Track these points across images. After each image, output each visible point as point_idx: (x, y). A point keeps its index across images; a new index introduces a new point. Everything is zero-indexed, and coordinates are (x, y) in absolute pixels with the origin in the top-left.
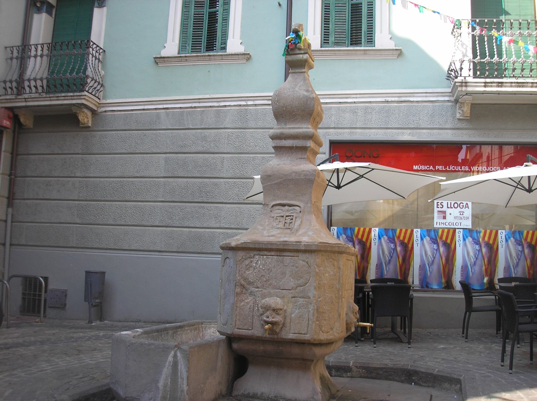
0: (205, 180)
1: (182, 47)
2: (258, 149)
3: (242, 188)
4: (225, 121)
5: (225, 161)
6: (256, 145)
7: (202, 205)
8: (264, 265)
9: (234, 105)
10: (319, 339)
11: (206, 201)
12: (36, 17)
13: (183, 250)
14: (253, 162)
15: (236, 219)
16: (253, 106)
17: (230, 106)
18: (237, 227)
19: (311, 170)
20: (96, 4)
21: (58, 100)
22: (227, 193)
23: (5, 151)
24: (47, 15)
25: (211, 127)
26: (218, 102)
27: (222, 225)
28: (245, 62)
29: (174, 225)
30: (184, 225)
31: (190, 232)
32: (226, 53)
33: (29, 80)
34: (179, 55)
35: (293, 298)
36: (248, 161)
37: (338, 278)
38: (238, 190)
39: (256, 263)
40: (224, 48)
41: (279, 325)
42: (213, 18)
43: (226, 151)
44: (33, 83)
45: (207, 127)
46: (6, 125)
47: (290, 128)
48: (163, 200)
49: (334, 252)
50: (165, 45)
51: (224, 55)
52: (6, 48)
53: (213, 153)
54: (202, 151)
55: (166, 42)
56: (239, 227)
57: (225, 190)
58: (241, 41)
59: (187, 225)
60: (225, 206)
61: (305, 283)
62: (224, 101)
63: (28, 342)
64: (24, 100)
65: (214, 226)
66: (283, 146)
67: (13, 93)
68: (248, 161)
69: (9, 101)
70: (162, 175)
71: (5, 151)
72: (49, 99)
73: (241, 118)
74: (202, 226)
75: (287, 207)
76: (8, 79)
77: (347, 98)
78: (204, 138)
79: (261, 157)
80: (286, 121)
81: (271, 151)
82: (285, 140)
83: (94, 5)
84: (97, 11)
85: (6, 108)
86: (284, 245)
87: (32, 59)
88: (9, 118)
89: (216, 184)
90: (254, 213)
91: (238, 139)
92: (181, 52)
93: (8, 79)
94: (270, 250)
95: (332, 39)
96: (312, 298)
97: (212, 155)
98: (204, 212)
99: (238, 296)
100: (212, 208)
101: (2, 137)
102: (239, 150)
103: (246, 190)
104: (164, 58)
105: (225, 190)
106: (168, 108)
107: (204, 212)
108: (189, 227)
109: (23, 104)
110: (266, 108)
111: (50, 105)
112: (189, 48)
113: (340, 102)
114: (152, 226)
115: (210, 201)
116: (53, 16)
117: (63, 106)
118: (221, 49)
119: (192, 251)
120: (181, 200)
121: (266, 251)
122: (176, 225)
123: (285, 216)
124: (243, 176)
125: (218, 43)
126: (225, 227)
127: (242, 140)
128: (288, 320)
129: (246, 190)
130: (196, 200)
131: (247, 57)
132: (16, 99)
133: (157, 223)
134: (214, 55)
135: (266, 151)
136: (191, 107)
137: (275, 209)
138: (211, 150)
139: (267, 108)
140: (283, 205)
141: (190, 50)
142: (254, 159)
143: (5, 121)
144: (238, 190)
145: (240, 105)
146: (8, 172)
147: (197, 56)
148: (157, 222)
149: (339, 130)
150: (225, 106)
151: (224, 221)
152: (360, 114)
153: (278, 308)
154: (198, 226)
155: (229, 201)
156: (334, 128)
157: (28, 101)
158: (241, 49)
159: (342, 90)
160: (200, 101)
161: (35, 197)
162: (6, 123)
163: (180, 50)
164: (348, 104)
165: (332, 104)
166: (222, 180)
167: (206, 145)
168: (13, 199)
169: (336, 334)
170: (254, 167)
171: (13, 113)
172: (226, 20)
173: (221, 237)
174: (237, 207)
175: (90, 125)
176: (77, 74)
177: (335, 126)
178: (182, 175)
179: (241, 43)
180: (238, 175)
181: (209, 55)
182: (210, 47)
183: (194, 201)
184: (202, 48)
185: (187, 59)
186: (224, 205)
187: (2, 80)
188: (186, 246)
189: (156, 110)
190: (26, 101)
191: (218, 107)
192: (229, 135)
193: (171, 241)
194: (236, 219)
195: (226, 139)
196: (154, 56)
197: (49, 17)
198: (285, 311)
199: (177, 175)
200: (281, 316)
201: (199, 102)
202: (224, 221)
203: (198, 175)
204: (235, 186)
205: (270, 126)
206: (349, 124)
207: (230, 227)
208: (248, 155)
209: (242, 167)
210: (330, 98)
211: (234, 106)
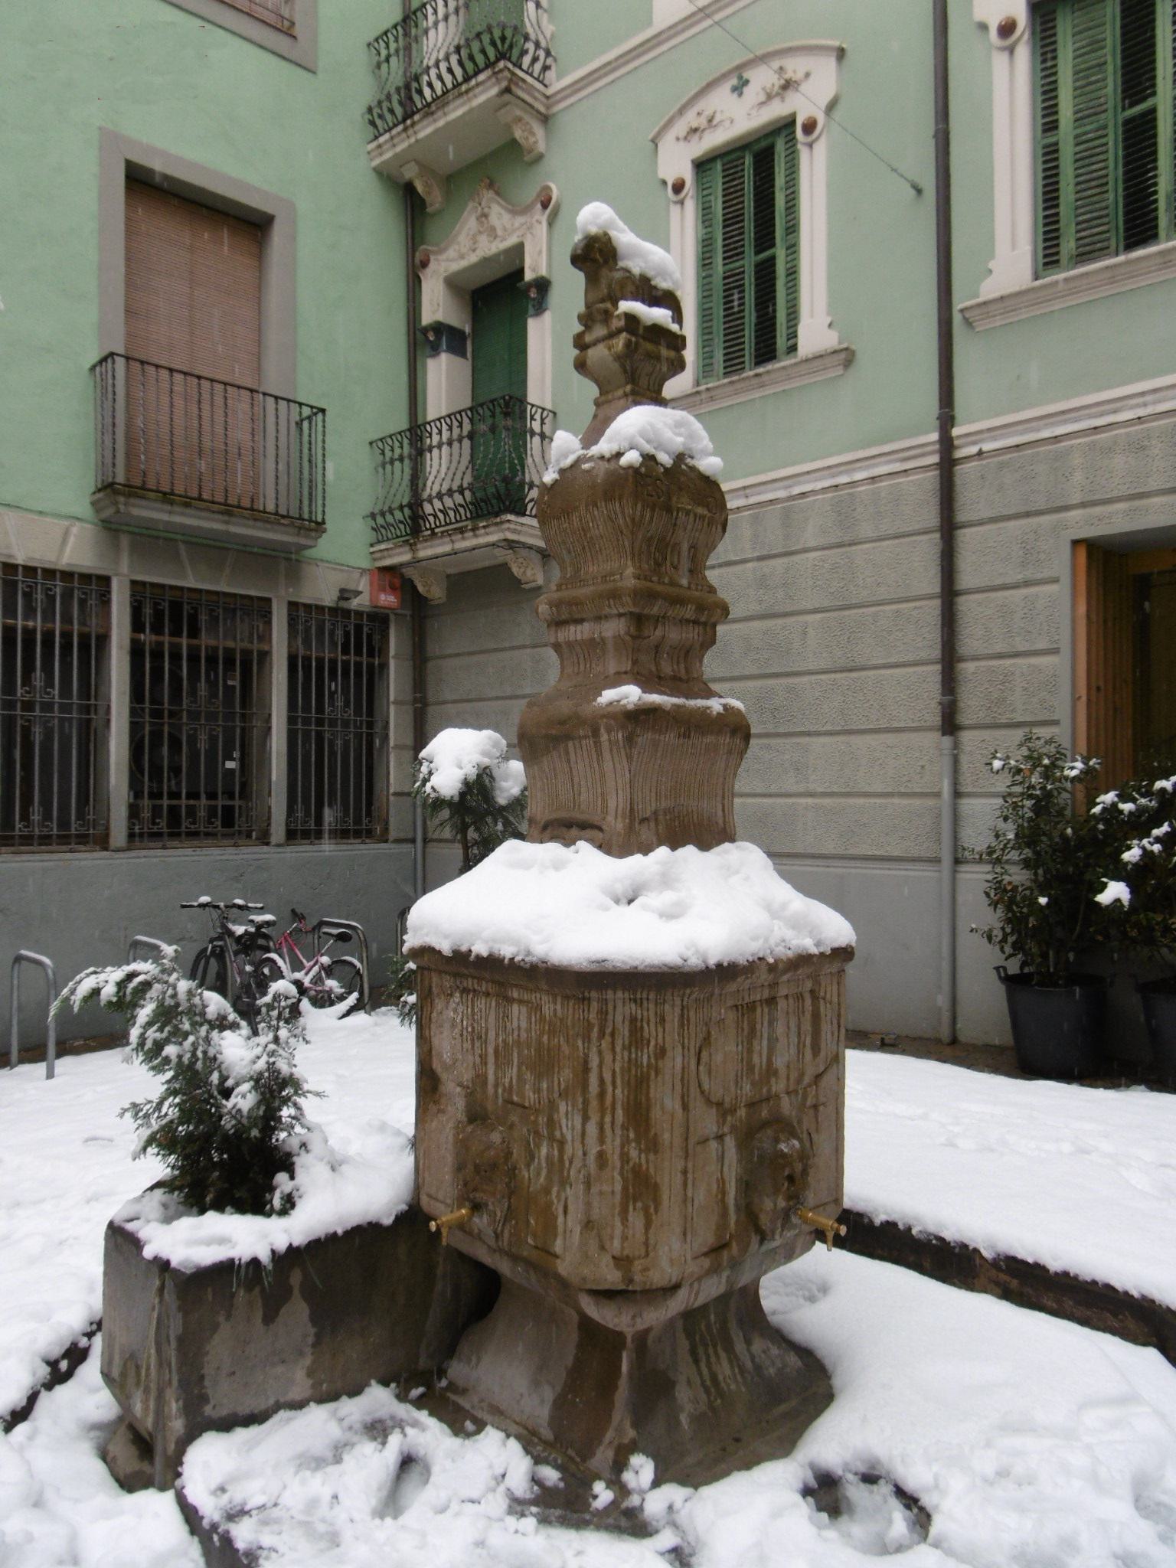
11: (773, 731)
12: (431, 364)
15: (841, 770)
17: (813, 492)
20: (531, 311)
24: (452, 357)
27: (812, 787)
32: (798, 359)
33: (430, 501)
40: (793, 349)
41: (1071, 258)
42: (766, 273)
44: (438, 504)
51: (795, 364)
52: (371, 443)
53: (785, 615)
56: (848, 790)
58: (829, 320)
65: (795, 789)
67: (380, 538)
76: (376, 511)
77: (1115, 412)
83: (526, 312)
84: (532, 324)
87: (435, 451)
88: (393, 589)
93: (376, 511)
95: (1068, 245)
97: (780, 621)
101: (388, 628)
113: (1095, 428)
115: (781, 730)
116: (469, 355)
125: (781, 342)
134: (768, 372)
141: (722, 371)
143: (383, 597)
146: (409, 697)
149: (1098, 510)
152: (1157, 451)
156: (1083, 505)
158: (829, 340)
159: (1100, 389)
164: (1119, 428)
165: (1071, 439)
166: (805, 679)
172: (793, 273)
175: (540, 581)
177: (1085, 500)
181: (757, 375)
182: (766, 352)
184: (747, 358)
194: (841, 770)
197: (458, 360)
202: (814, 777)
206: (1126, 486)
208: (861, 611)
211: (824, 490)
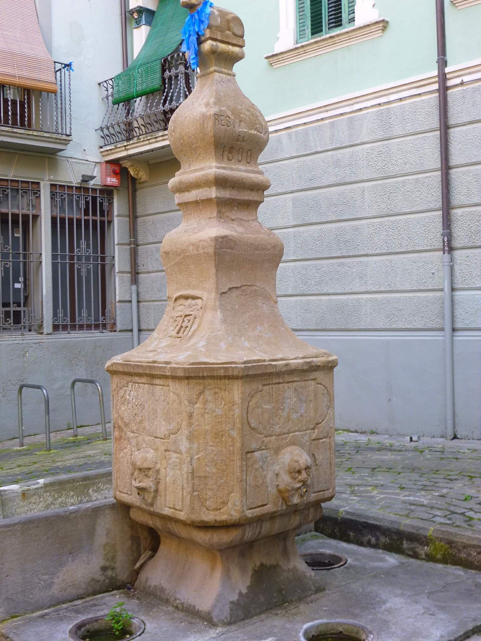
0: (311, 228)
1: (301, 34)
2: (408, 168)
3: (390, 230)
4: (361, 132)
5: (366, 192)
6: (406, 161)
7: (342, 260)
8: (137, 398)
9: (372, 106)
10: (201, 521)
13: (324, 327)
14: (403, 189)
16: (397, 102)
17: (366, 108)
18: (388, 290)
19: (209, 238)
21: (157, 142)
22: (372, 240)
23: (118, 216)
25: (343, 145)
26: (350, 105)
27: (370, 288)
28: (381, 35)
29: (310, 292)
30: (322, 292)
31: (330, 300)
34: (299, 45)
35: (167, 452)
36: (397, 188)
37: (231, 420)
38: (386, 233)
39: (129, 395)
40: (352, 20)
43: (366, 178)
45: (338, 146)
46: (110, 183)
47: (196, 170)
48: (295, 258)
49: (220, 378)
50: (278, 36)
52: (99, 84)
54: (336, 183)
55: (279, 31)
56: (391, 289)
57: (369, 236)
59: (325, 291)
60: (370, 260)
61: (177, 430)
62: (358, 103)
63: (97, 463)
64: (124, 148)
66: (186, 201)
68: (397, 188)
69: (110, 152)
70: (291, 224)
71: (118, 216)
72: (147, 142)
73: (381, 123)
74: (344, 291)
75: (189, 301)
78: (337, 163)
79: (413, 179)
80: (190, 161)
81: (427, 169)
82: (188, 191)
85: (107, 162)
86: (150, 367)
88: (115, 173)
89: (356, 229)
90: (410, 267)
91: (381, 157)
92: (300, 41)
93: (103, 126)
94: (140, 375)
96: (184, 453)
97: (348, 187)
98: (344, 270)
99: (118, 443)
100: (355, 264)
102: (383, 173)
103: (397, 233)
104: (276, 55)
105: (369, 236)
106: (290, 127)
107: (344, 270)
108: (329, 294)
109: (124, 154)
110: (415, 102)
111: (152, 150)
112: (309, 31)
114: (285, 296)
115: (351, 254)
117: (165, 149)
118: (349, 22)
119: (333, 328)
120: (316, 256)
121: (137, 376)
122: (313, 293)
123: (183, 316)
124: (391, 212)
125: (345, 16)
126: (372, 290)
127: (386, 158)
128: (161, 487)
129: (397, 233)
130: (334, 255)
131: (383, 25)
132: (116, 148)
133: (290, 292)
134: (338, 35)
135: (419, 170)
136: (318, 120)
137: (178, 304)
138: (348, 180)
139: (417, 102)
140: (187, 298)
142: (404, 184)
144: (386, 233)
145: (380, 104)
147: (316, 42)
148: (291, 290)
150: (360, 109)
151: (370, 282)
153: (144, 467)
154: (339, 291)
155: (376, 252)
157: (129, 149)
158: (374, 16)
160: (328, 108)
161: (159, 269)
162: (111, 181)
163: (299, 38)
166: (364, 222)
167: (340, 173)
168: (138, 273)
169: (233, 513)
170: (405, 197)
171: (120, 165)
173: (368, 306)
174: (387, 260)
176: (170, 104)
178: (314, 221)
179: (373, 6)
180: (385, 212)
183: (331, 255)
185: (305, 49)
186: (370, 258)
187: (98, 128)
188: (326, 321)
189: (277, 132)
190: (127, 150)
191: (351, 112)
192: (368, 153)
193: (309, 316)
195: (365, 159)
196: (265, 56)
198: (158, 471)
199: (309, 222)
200: (151, 479)
201: (327, 111)
202: (370, 282)
203: (334, 218)
204: (382, 228)
205: (423, 129)
207: (380, 290)
209: (389, 199)
210: (470, 73)
